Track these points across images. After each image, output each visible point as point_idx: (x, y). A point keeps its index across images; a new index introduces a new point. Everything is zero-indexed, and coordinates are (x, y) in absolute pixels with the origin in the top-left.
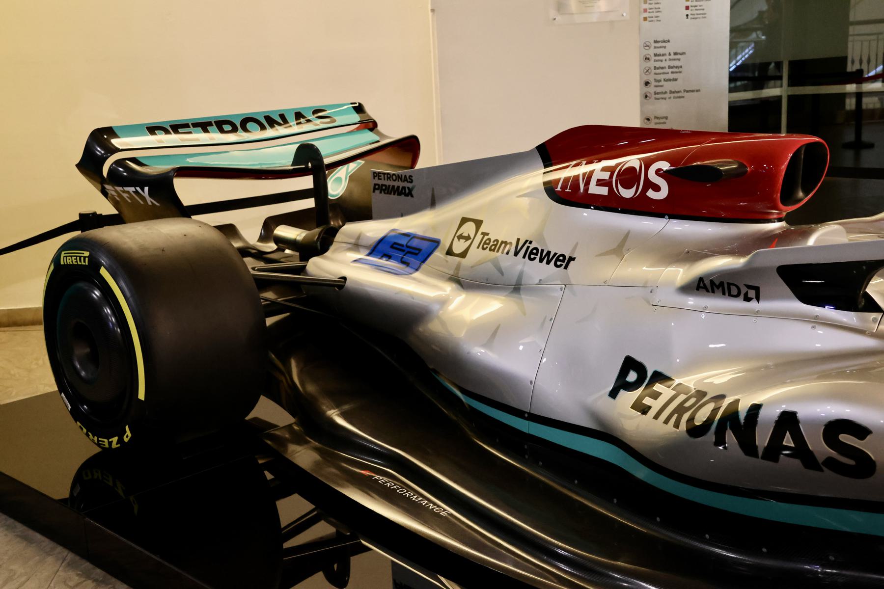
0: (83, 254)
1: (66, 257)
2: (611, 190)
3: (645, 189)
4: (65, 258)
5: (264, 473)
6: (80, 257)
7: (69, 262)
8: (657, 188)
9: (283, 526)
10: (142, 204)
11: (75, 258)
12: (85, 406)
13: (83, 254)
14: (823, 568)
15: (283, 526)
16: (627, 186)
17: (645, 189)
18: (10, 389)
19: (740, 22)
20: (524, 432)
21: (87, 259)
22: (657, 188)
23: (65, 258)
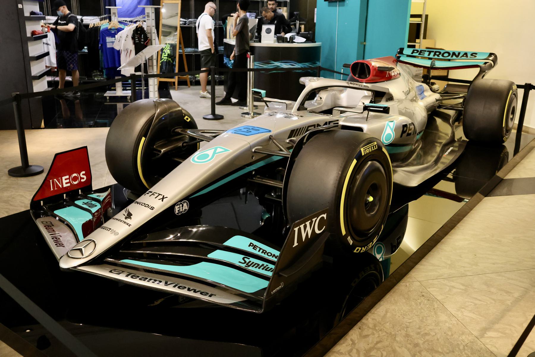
0: (374, 144)
1: (365, 150)
2: (71, 184)
3: (80, 180)
4: (365, 151)
5: (231, 99)
6: (373, 146)
7: (368, 152)
8: (83, 178)
9: (463, 99)
10: (41, 97)
11: (371, 148)
12: (279, 304)
13: (374, 144)
14: (75, 96)
15: (463, 99)
16: (75, 177)
17: (80, 180)
18: (389, 315)
19: (149, 4)
20: (533, 318)
21: (376, 146)
22: (83, 178)
23: (365, 151)
